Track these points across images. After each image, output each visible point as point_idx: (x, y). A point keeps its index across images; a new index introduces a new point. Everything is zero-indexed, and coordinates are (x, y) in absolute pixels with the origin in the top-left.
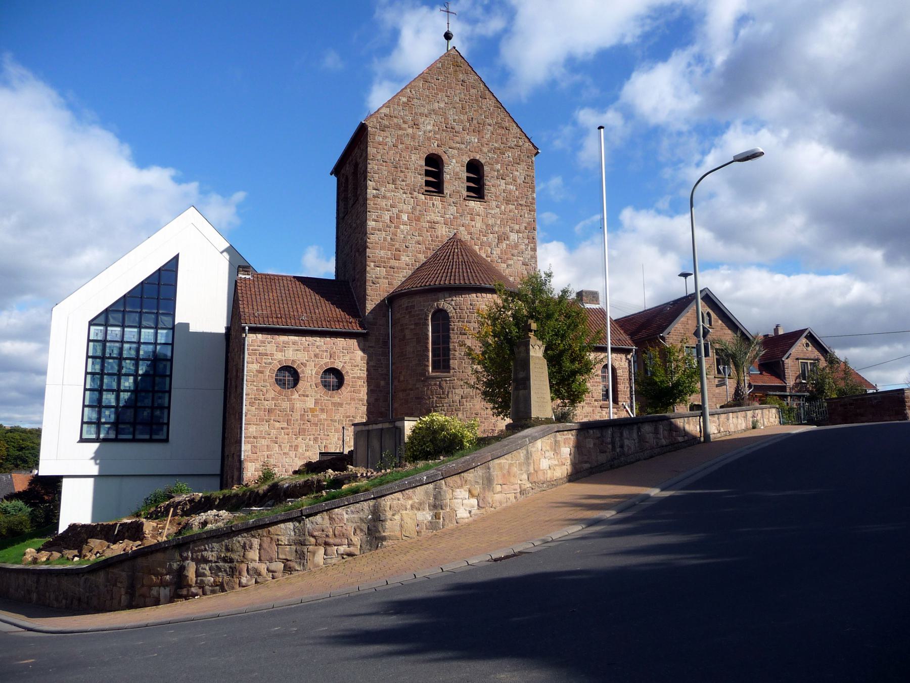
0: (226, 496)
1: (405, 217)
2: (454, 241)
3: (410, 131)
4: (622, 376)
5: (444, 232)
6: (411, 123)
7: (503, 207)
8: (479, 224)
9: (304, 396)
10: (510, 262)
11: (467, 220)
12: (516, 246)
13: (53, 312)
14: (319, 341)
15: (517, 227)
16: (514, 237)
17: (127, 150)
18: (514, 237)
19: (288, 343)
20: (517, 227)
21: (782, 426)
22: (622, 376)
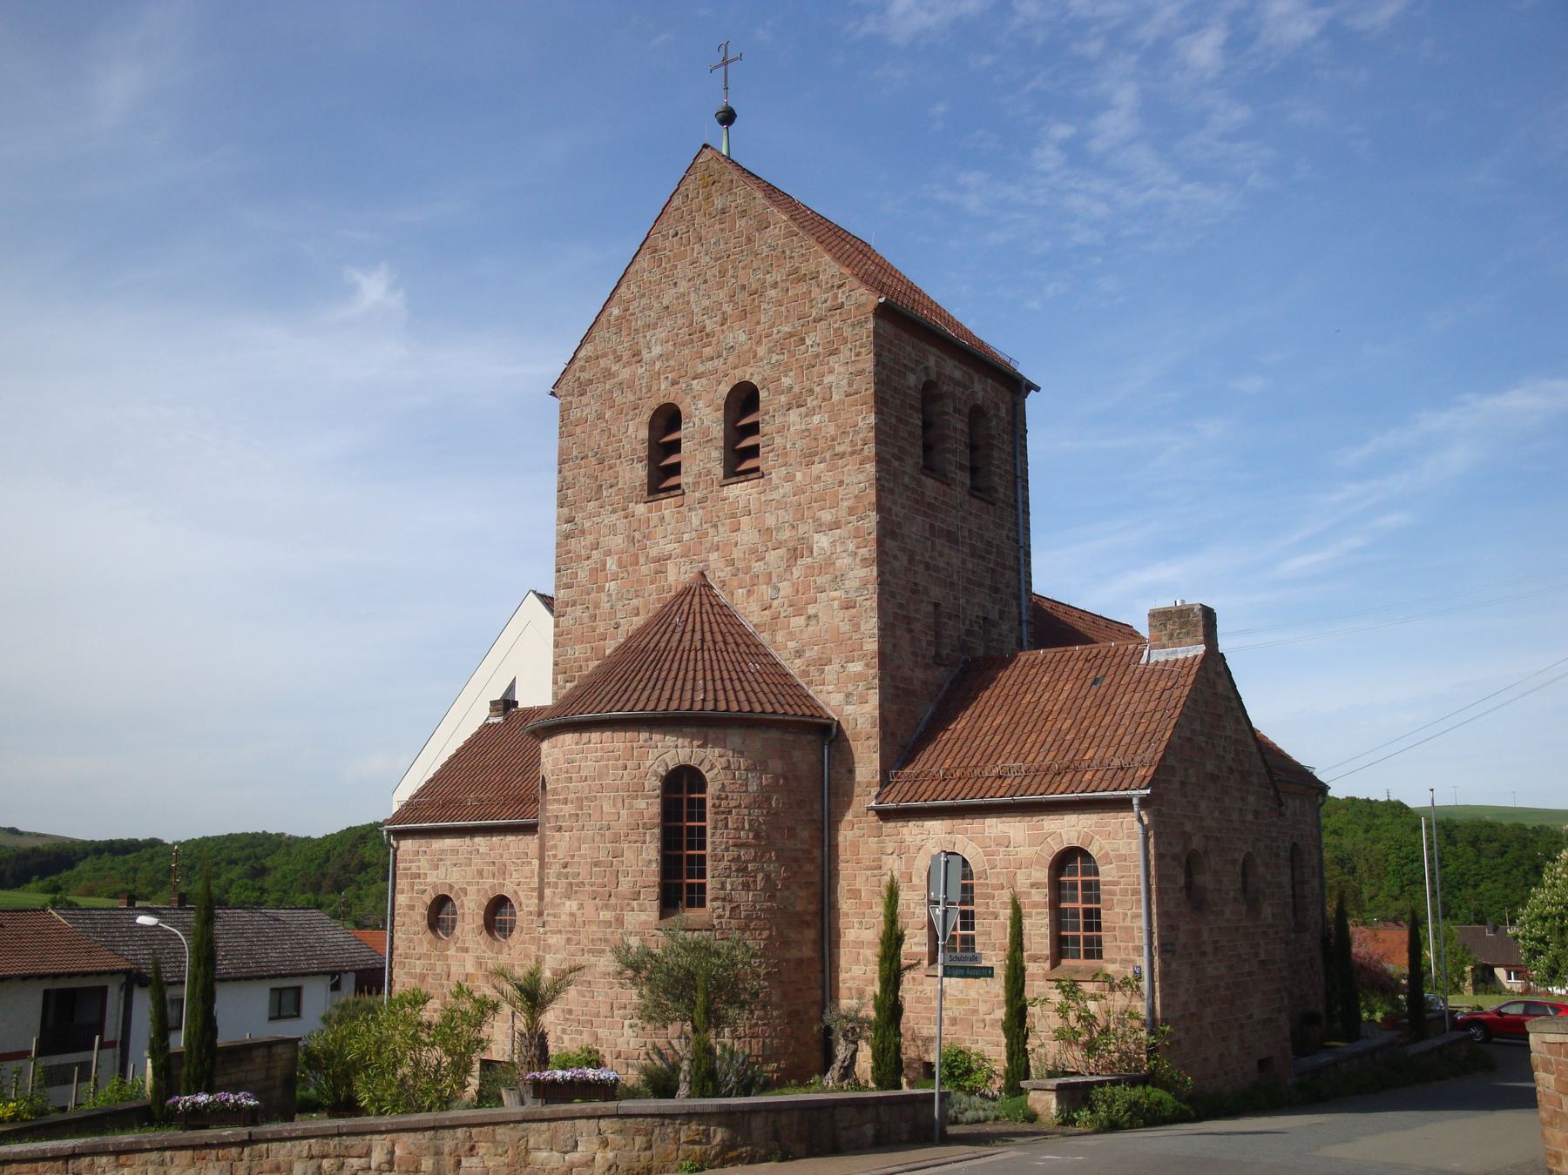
0: (878, 993)
1: (611, 564)
2: (702, 586)
3: (625, 374)
4: (1116, 883)
5: (678, 576)
6: (626, 356)
7: (799, 476)
8: (748, 536)
9: (462, 951)
10: (811, 610)
11: (723, 534)
12: (829, 562)
13: (21, 829)
14: (448, 843)
15: (826, 516)
16: (822, 542)
17: (1506, 823)
18: (822, 542)
19: (443, 851)
20: (826, 516)
21: (1195, 599)
22: (1116, 883)
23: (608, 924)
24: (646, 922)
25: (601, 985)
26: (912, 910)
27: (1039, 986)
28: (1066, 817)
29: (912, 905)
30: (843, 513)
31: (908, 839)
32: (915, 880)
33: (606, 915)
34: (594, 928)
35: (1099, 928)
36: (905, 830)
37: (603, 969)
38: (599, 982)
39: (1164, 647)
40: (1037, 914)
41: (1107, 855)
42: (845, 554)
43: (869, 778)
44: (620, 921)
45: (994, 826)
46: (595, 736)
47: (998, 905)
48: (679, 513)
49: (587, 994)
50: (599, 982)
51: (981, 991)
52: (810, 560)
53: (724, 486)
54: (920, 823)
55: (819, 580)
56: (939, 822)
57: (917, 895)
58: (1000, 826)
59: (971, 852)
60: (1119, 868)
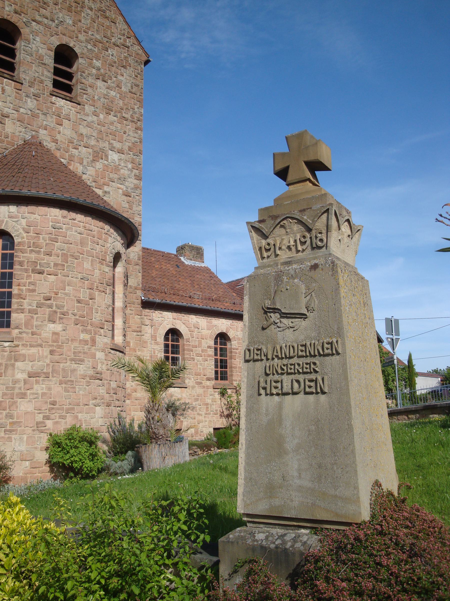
4: (237, 349)
15: (117, 145)
18: (114, 156)
22: (237, 349)
23: (86, 342)
24: (106, 344)
25: (82, 384)
26: (156, 354)
27: (210, 391)
28: (221, 320)
29: (156, 352)
30: (126, 148)
31: (155, 318)
32: (158, 340)
33: (84, 336)
34: (76, 344)
35: (226, 367)
36: (154, 314)
37: (82, 372)
38: (80, 382)
39: (191, 260)
40: (210, 359)
41: (234, 337)
42: (126, 168)
43: (136, 285)
44: (93, 341)
45: (193, 319)
46: (80, 217)
47: (195, 355)
48: (18, 93)
49: (71, 390)
50: (80, 382)
51: (188, 394)
52: (106, 162)
53: (53, 95)
54: (161, 312)
55: (112, 175)
56: (170, 313)
57: (160, 347)
58: (195, 319)
59: (182, 329)
60: (238, 343)
